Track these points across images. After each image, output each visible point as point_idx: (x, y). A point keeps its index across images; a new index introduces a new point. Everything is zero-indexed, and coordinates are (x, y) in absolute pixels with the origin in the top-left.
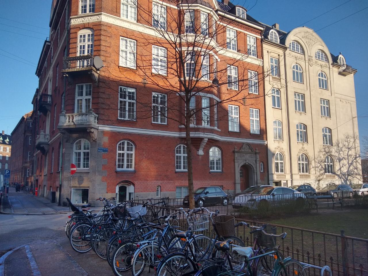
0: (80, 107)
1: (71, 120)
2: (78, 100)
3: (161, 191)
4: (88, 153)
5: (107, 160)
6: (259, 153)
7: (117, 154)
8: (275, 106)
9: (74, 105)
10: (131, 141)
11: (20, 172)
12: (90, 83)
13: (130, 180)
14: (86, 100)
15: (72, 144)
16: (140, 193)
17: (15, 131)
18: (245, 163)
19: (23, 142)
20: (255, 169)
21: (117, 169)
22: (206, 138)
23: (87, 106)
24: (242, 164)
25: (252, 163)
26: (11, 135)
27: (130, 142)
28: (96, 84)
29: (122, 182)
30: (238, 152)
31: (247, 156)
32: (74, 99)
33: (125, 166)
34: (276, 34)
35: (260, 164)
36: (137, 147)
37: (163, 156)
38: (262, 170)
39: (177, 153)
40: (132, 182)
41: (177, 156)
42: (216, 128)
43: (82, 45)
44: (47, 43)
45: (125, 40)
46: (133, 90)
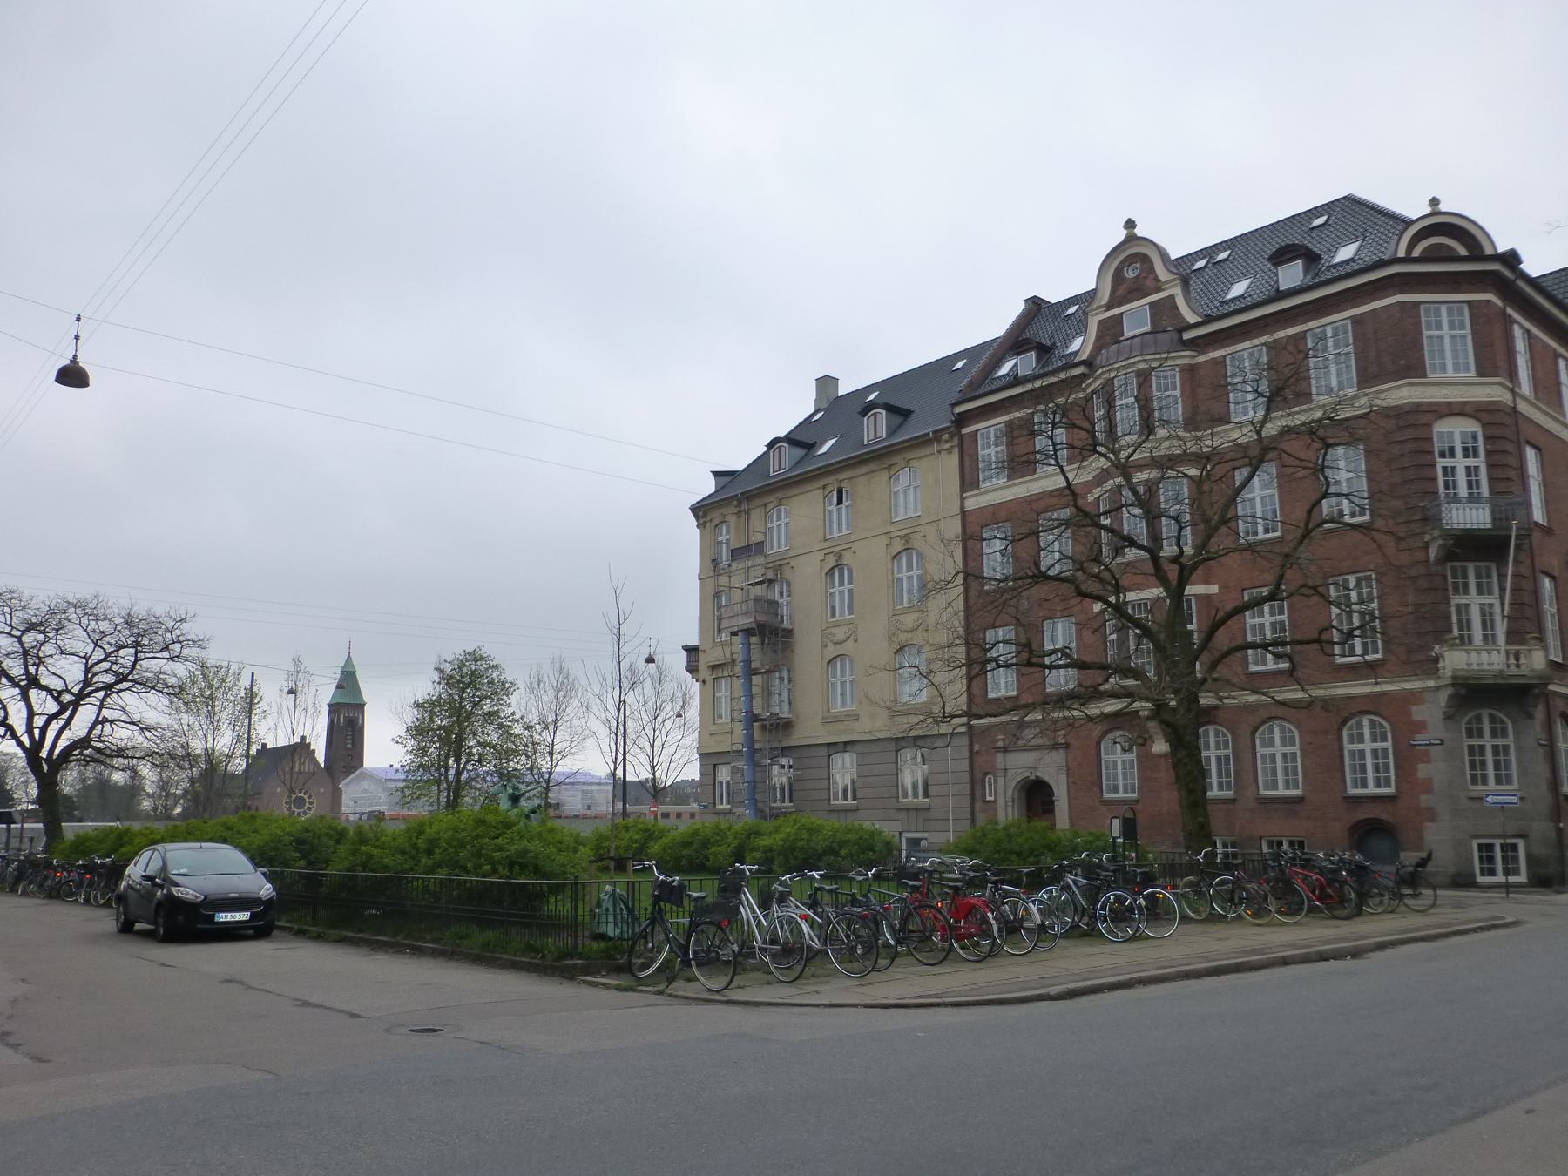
0: (1465, 625)
23: (1487, 624)
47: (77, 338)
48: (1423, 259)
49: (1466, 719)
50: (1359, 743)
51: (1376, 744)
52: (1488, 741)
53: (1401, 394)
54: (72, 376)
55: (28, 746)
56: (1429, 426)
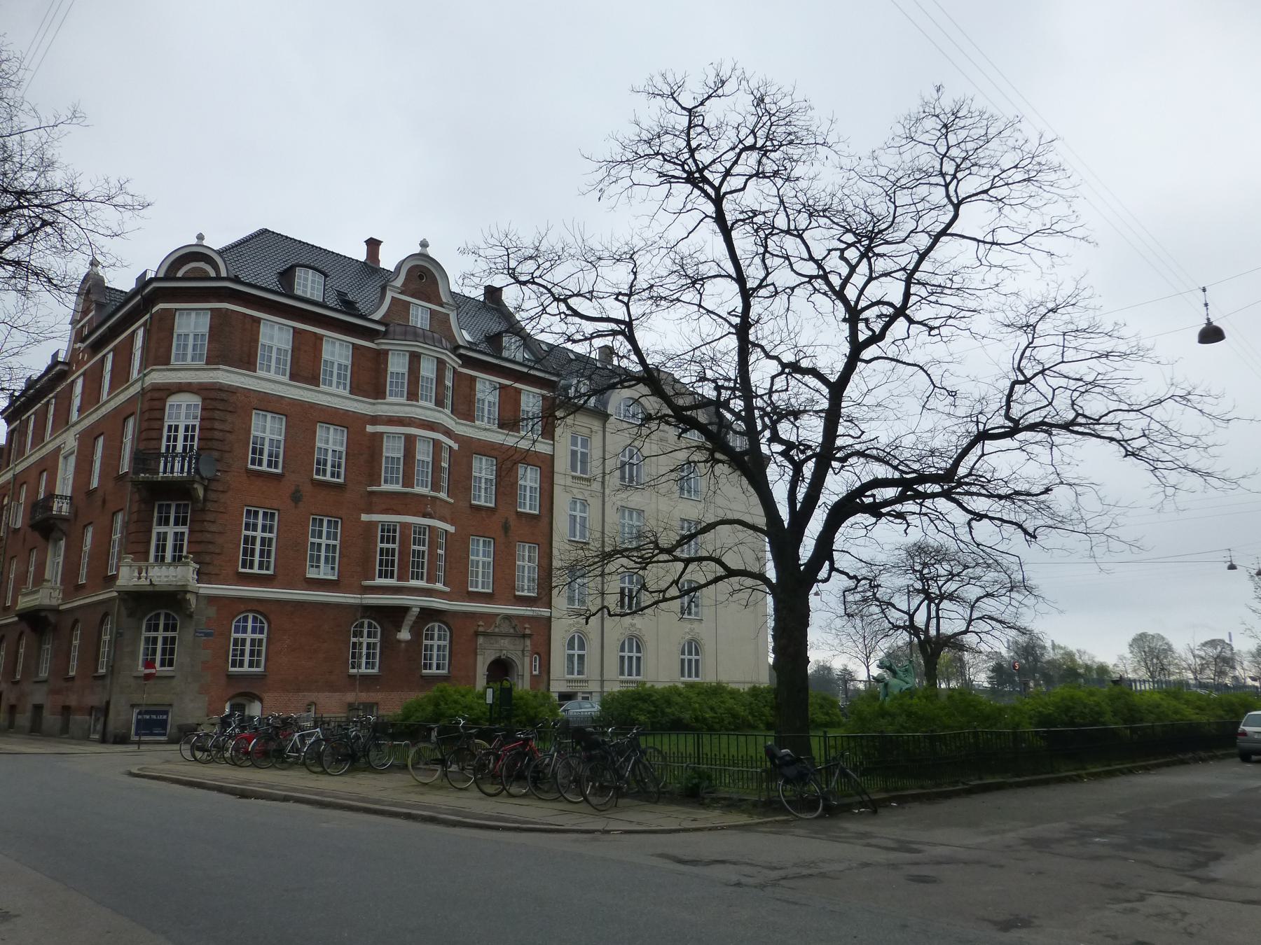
0: (161, 548)
1: (144, 574)
2: (159, 534)
4: (173, 639)
6: (530, 636)
9: (149, 542)
10: (261, 613)
12: (186, 502)
14: (176, 534)
15: (141, 619)
20: (520, 667)
21: (231, 669)
22: (416, 606)
23: (178, 548)
24: (493, 658)
27: (259, 617)
30: (485, 634)
31: (505, 642)
32: (150, 531)
33: (246, 663)
35: (531, 657)
36: (272, 626)
39: (313, 536)
43: (173, 424)
46: (312, 574)
47: (1206, 305)
49: (148, 617)
50: (154, 631)
51: (255, 635)
53: (227, 377)
54: (1211, 334)
55: (774, 581)
56: (164, 401)
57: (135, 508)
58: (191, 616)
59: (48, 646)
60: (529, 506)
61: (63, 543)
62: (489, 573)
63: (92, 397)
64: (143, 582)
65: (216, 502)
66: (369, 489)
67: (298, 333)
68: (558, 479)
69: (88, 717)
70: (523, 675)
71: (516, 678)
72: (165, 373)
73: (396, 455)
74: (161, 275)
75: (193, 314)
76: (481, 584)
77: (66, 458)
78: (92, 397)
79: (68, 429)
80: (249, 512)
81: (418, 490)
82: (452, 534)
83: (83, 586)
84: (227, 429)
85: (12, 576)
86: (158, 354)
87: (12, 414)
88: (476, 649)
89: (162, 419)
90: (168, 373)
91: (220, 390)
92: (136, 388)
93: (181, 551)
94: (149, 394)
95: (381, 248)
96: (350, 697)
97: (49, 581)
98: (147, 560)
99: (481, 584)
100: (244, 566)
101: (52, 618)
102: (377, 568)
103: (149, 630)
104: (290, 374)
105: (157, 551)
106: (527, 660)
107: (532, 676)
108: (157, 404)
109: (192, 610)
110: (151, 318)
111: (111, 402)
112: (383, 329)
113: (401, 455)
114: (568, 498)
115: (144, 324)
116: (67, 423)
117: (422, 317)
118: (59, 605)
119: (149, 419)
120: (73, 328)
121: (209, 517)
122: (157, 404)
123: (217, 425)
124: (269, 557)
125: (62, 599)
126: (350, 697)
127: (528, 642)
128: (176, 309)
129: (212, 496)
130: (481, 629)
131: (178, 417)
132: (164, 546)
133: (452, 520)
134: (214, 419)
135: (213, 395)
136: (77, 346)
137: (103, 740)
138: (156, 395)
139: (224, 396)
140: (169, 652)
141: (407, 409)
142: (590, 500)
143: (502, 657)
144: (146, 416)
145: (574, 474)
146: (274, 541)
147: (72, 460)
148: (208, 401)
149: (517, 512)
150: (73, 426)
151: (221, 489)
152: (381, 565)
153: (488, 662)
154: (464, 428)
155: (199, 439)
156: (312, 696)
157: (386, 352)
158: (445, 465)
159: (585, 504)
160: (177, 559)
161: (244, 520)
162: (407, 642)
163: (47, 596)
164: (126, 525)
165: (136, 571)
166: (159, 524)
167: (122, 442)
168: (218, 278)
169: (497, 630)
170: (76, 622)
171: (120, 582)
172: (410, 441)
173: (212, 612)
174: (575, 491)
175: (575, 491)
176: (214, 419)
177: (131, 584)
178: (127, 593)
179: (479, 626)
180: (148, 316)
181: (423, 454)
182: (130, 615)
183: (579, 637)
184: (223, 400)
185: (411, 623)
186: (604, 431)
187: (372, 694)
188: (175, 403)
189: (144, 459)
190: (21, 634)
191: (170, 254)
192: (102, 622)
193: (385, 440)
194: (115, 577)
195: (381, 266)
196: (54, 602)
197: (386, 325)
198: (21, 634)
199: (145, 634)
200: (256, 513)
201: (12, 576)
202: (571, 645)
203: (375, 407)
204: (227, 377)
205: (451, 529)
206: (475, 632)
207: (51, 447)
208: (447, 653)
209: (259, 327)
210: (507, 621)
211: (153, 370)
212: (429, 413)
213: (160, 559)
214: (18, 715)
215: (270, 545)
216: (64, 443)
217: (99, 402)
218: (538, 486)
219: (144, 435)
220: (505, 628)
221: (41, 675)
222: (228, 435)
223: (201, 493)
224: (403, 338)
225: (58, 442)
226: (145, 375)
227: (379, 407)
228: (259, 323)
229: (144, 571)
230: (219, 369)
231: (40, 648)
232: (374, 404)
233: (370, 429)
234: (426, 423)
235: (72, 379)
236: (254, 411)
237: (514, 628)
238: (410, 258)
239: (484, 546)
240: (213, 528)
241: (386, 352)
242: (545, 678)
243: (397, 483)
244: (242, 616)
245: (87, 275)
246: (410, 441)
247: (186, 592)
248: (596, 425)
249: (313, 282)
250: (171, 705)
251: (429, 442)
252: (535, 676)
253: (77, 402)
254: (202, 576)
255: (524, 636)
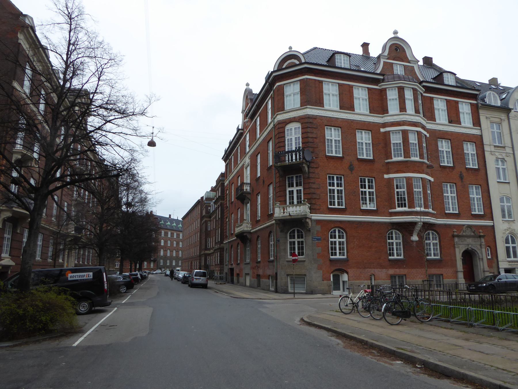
1: (285, 211)
2: (289, 191)
3: (374, 280)
4: (302, 242)
5: (321, 248)
6: (483, 236)
7: (330, 242)
8: (499, 177)
9: (286, 196)
10: (342, 228)
11: (197, 260)
13: (343, 268)
14: (297, 190)
15: (287, 233)
16: (354, 281)
17: (187, 216)
18: (468, 248)
19: (199, 228)
20: (480, 255)
23: (299, 198)
24: (464, 249)
25: (476, 248)
26: (181, 220)
27: (341, 230)
28: (306, 175)
29: (336, 270)
30: (458, 236)
31: (469, 241)
32: (286, 191)
34: (495, 95)
36: (348, 234)
37: (375, 243)
38: (489, 256)
40: (346, 270)
41: (389, 243)
42: (430, 210)
44: (240, 131)
45: (330, 128)
46: (364, 207)
48: (286, 68)
52: (337, 240)
53: (311, 111)
57: (278, 180)
58: (309, 231)
59: (248, 248)
60: (472, 164)
61: (249, 205)
62: (455, 202)
63: (253, 138)
64: (286, 214)
65: (314, 173)
66: (386, 161)
67: (341, 85)
68: (486, 148)
69: (268, 280)
70: (482, 259)
71: (478, 260)
72: (283, 115)
73: (398, 142)
74: (276, 69)
75: (292, 85)
76: (452, 207)
77: (246, 168)
78: (253, 138)
79: (246, 156)
80: (329, 177)
81: (413, 159)
82: (432, 182)
83: (259, 220)
84: (315, 137)
85: (232, 221)
86: (279, 107)
87: (226, 158)
88: (454, 245)
89: (284, 137)
90: (284, 115)
91: (309, 118)
92: (272, 125)
93: (301, 199)
94: (277, 127)
95: (369, 46)
96: (391, 272)
97: (246, 220)
98: (286, 204)
99: (452, 207)
100: (331, 205)
101: (249, 236)
102: (396, 202)
103: (290, 238)
104: (340, 106)
105: (290, 200)
106: (484, 250)
107: (488, 259)
108: (281, 130)
109: (310, 227)
110: (274, 92)
111: (260, 136)
112: (382, 77)
113: (401, 141)
114: (494, 158)
115: (271, 97)
116: (245, 153)
117: (400, 70)
118: (251, 230)
119: (279, 138)
120: (243, 114)
121: (312, 181)
122: (281, 130)
123: (310, 135)
124: (342, 199)
125: (252, 228)
126: (391, 272)
127: (483, 240)
128: (284, 84)
129: (311, 170)
130: (455, 234)
131: (291, 135)
132: (293, 197)
133: (431, 174)
134: (308, 132)
135: (306, 120)
136: (245, 121)
137: (276, 291)
138: (280, 126)
139: (311, 120)
140: (301, 248)
141: (401, 117)
142: (506, 158)
143: (469, 249)
144: (277, 137)
145: (495, 144)
146: (343, 191)
147: (249, 168)
148: (304, 124)
149: (466, 168)
150: (247, 154)
151: (315, 166)
152: (398, 201)
153: (462, 252)
154: (431, 125)
155: (302, 143)
156: (372, 271)
157: (385, 90)
158: (424, 145)
159: (503, 160)
160: (299, 203)
161: (328, 181)
162: (416, 242)
163: (246, 227)
164: (274, 189)
165: (282, 209)
166: (289, 187)
167: (268, 153)
168: (301, 64)
169: (464, 234)
170: (258, 237)
171: (276, 215)
172: (405, 134)
173: (318, 228)
174: (497, 154)
175: (497, 154)
176: (308, 132)
177: (280, 216)
178: (279, 220)
179: (454, 232)
180: (272, 92)
181: (413, 139)
182: (282, 231)
183: (511, 236)
184: (311, 123)
185: (418, 231)
186: (509, 119)
187: (402, 270)
188: (289, 128)
189: (279, 156)
190: (238, 243)
191: (279, 59)
192: (269, 236)
193: (391, 135)
194: (272, 215)
195: (371, 56)
196: (249, 229)
197: (383, 75)
198: (238, 243)
199: (289, 240)
200: (333, 178)
201: (232, 221)
202: (507, 242)
203: (384, 119)
204: (311, 111)
205: (432, 180)
206: (452, 235)
207: (240, 165)
208: (438, 247)
209: (322, 85)
210: (469, 229)
211: (277, 115)
212: (412, 117)
213: (292, 203)
214: (240, 278)
215: (341, 193)
216: (245, 162)
217: (256, 139)
218: (475, 152)
219: (278, 146)
220: (469, 232)
221: (247, 261)
222: (315, 139)
223: (307, 169)
224: (393, 80)
225: (242, 163)
226: (274, 119)
227: (386, 118)
228: (322, 83)
229: (286, 209)
230: (307, 108)
231: (245, 249)
232: (382, 117)
233: (382, 130)
234: (412, 123)
235: (245, 135)
236: (326, 127)
237: (474, 232)
238: (389, 41)
239: (451, 188)
240: (314, 186)
241: (385, 90)
242: (495, 260)
243: (401, 156)
244: (333, 230)
245: (246, 89)
246: (405, 134)
247: (306, 218)
248: (503, 116)
249: (344, 60)
250: (305, 275)
251: (415, 133)
252: (489, 259)
253: (248, 144)
254: (312, 210)
255: (480, 237)
